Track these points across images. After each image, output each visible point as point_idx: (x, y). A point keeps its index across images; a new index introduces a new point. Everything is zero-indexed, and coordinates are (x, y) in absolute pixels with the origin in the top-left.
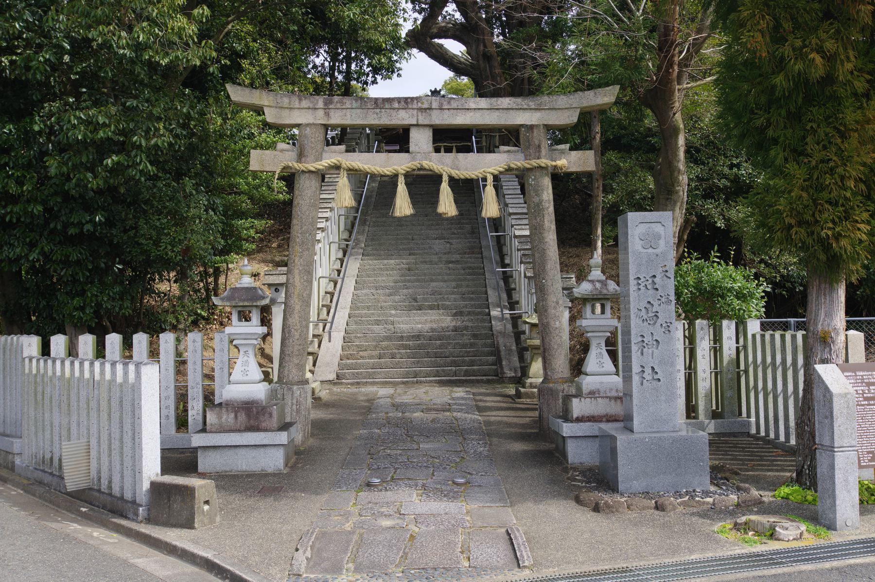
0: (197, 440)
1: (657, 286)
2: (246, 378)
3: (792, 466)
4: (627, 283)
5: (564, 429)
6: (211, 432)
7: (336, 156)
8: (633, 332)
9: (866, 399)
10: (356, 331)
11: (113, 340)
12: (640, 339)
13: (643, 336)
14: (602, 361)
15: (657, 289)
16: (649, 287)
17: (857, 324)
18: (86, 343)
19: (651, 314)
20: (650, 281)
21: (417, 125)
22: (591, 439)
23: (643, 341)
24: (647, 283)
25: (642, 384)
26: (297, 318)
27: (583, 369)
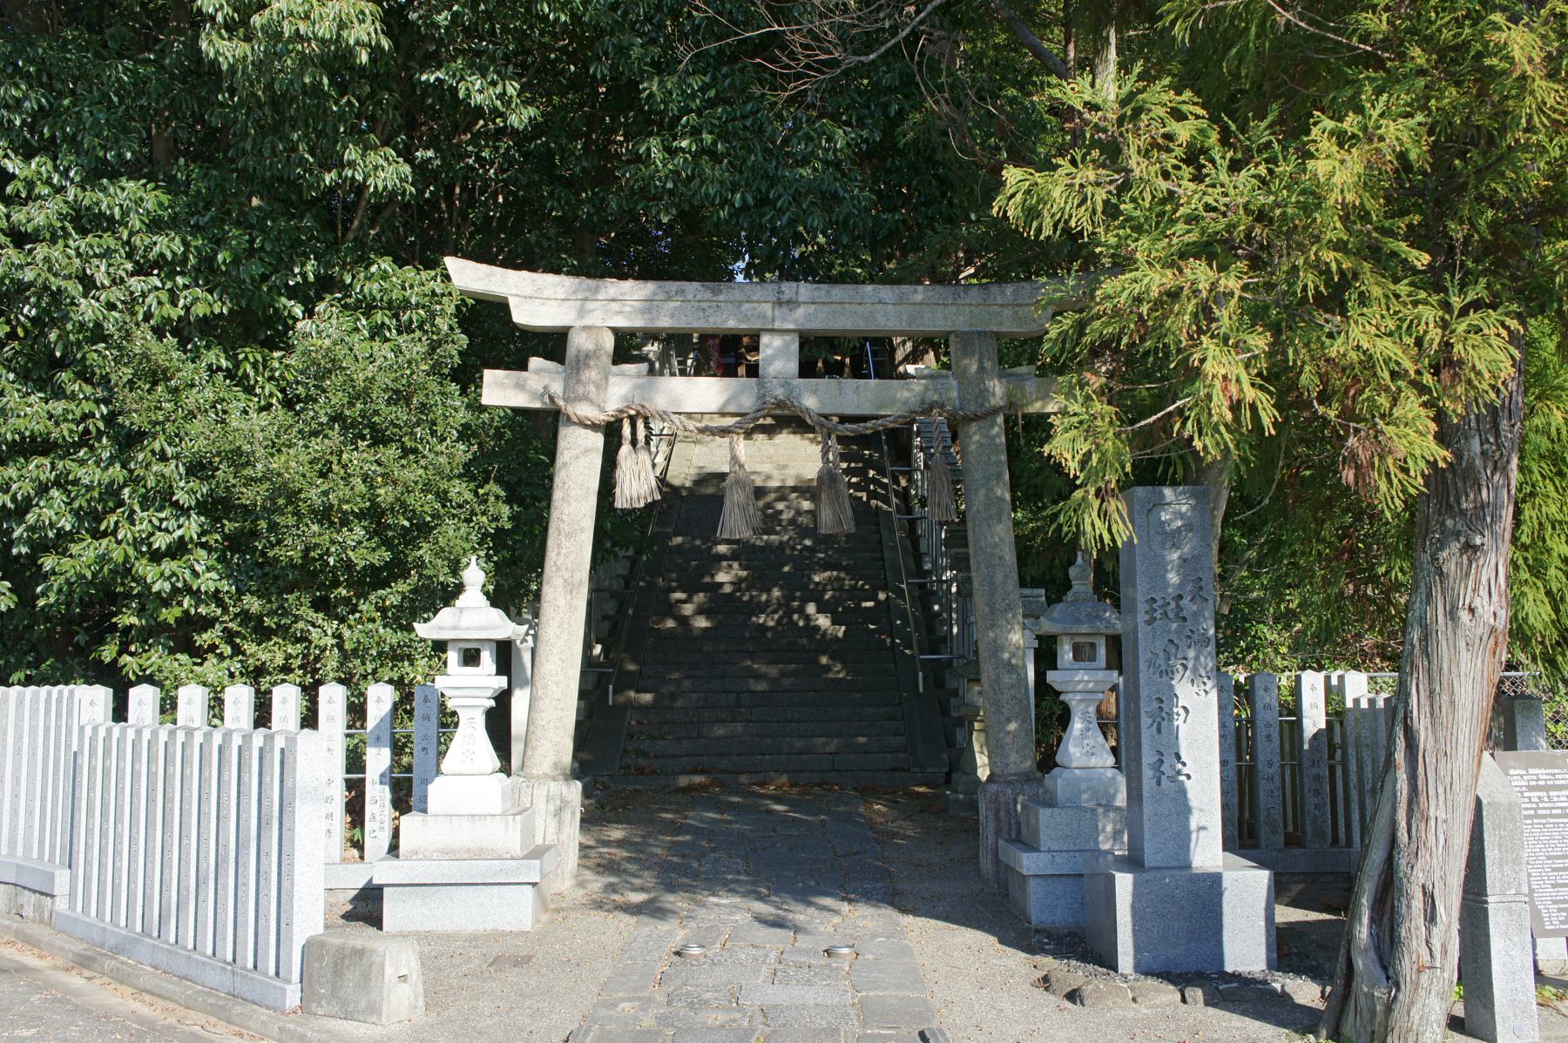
1: (1184, 613)
3: (28, 846)
4: (1133, 611)
5: (1025, 863)
8: (1144, 693)
11: (1364, 705)
15: (1184, 619)
16: (1171, 615)
25: (1159, 784)
27: (1058, 759)
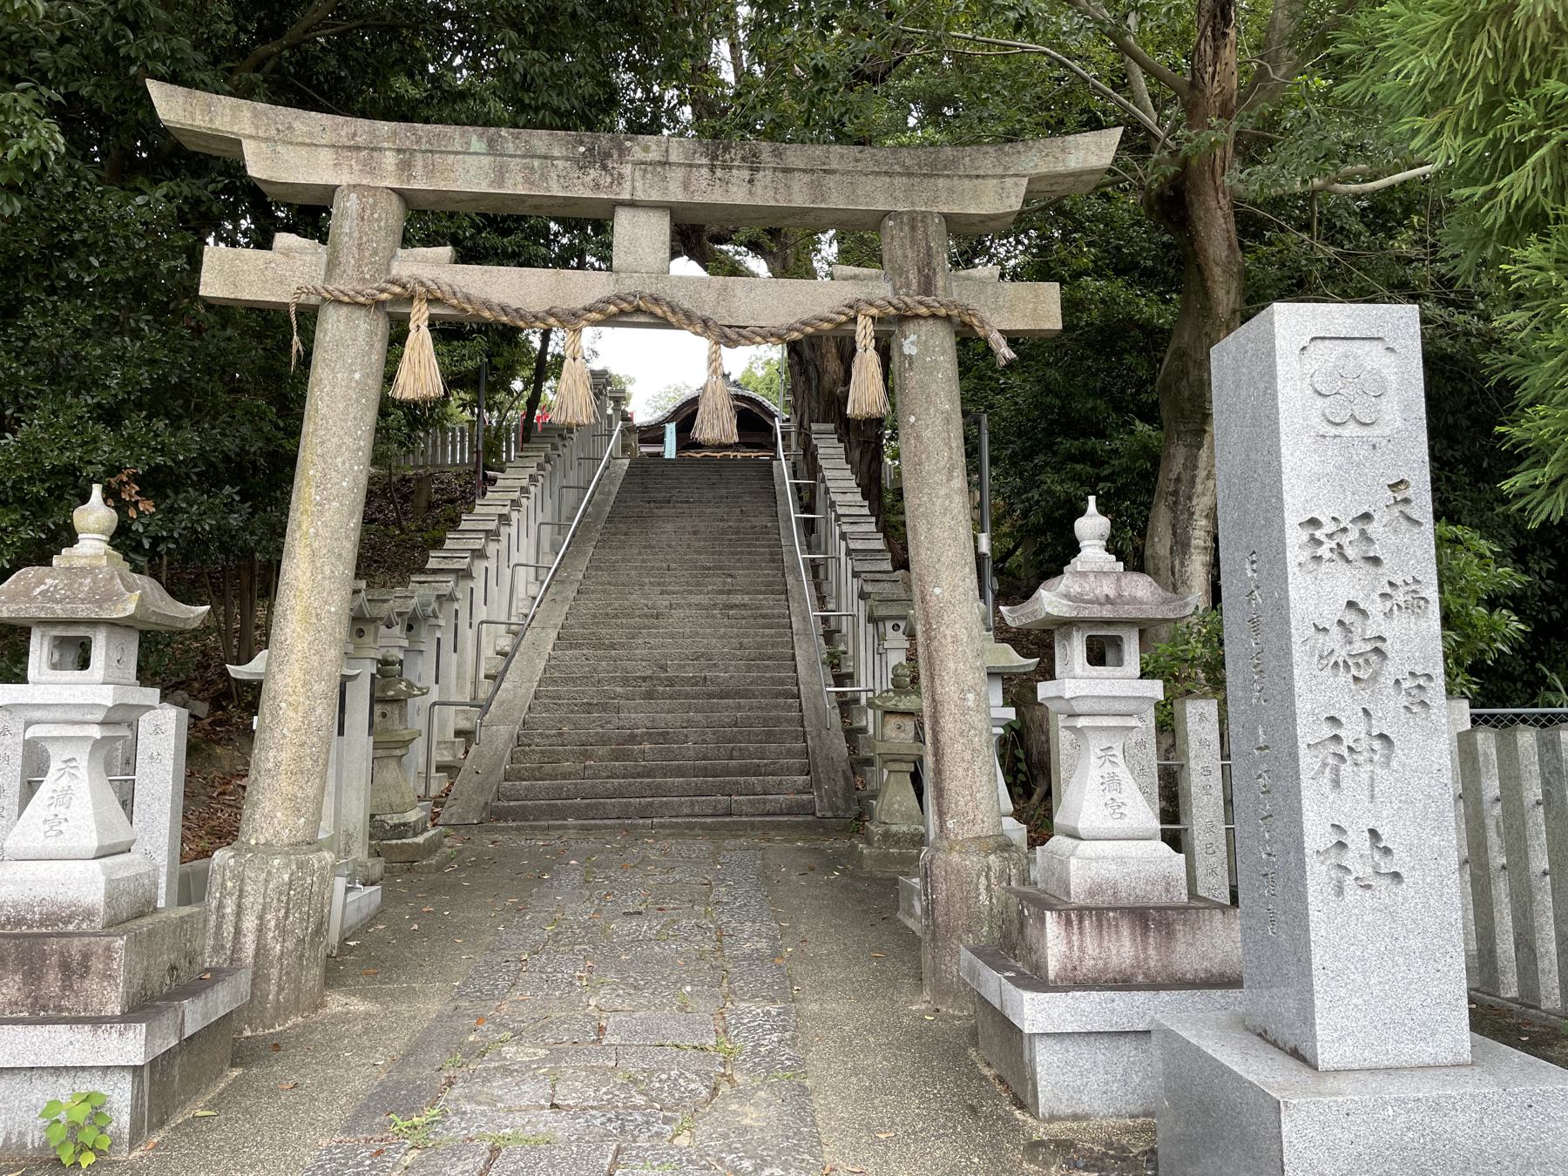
2: (53, 845)
7: (432, 266)
12: (1327, 731)
13: (1333, 720)
14: (1120, 798)
15: (1375, 561)
16: (1350, 552)
17: (1536, 721)
19: (1359, 647)
20: (1354, 534)
21: (632, 204)
22: (1106, 1041)
23: (1336, 738)
24: (1344, 540)
25: (1340, 890)
26: (298, 674)
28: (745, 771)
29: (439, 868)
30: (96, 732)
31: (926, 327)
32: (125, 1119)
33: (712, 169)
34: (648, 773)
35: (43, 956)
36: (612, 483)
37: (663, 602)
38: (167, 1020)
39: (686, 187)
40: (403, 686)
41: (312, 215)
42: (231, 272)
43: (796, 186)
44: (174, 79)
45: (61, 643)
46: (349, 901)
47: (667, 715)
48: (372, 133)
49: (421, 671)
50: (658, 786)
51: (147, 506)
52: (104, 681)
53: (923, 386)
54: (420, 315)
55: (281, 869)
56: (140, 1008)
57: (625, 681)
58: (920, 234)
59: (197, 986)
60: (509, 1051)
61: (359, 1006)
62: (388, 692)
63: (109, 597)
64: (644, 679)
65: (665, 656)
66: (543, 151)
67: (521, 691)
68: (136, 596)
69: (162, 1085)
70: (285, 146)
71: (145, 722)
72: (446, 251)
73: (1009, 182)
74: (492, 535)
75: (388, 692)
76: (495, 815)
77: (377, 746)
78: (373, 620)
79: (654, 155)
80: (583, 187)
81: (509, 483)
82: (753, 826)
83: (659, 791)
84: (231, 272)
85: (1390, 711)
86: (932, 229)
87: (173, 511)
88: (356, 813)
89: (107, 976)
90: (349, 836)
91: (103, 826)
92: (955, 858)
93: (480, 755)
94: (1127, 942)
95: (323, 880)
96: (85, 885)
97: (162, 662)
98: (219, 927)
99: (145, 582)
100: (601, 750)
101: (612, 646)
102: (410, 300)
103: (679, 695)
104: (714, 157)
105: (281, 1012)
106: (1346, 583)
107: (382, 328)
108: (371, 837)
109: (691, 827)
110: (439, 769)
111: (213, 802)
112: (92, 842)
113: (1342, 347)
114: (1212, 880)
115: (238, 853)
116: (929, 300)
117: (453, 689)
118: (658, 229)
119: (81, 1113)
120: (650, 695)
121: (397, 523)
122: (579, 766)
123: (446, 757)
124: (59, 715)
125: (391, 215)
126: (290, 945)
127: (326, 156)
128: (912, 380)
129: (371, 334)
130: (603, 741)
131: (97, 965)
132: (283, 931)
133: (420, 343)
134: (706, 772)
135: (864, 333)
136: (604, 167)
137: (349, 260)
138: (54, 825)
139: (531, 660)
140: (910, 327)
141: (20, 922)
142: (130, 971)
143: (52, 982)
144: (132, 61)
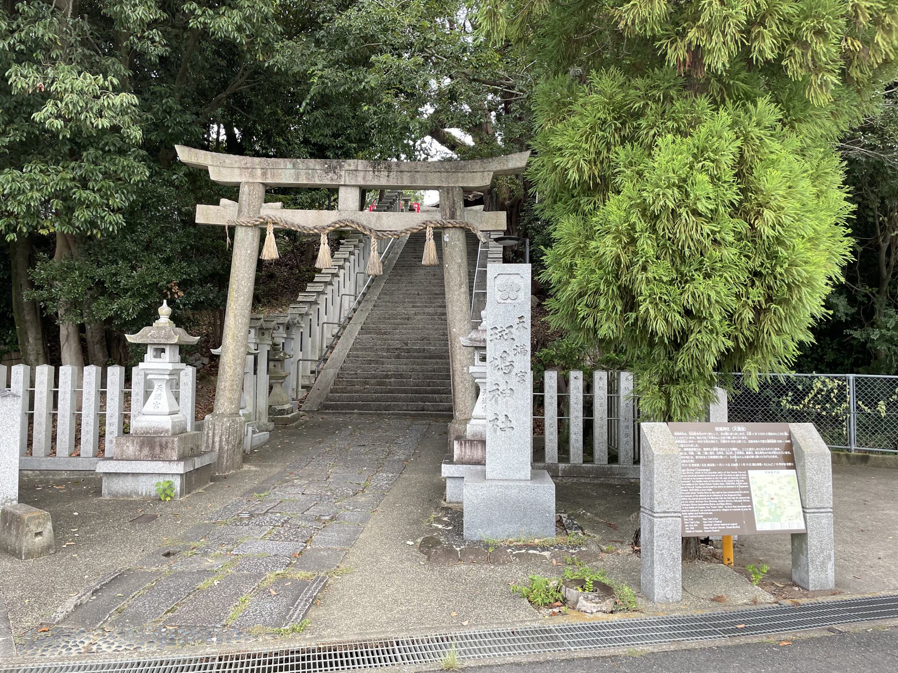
0: (103, 467)
2: (156, 410)
6: (111, 459)
7: (275, 211)
9: (697, 461)
10: (349, 369)
18: (42, 373)
25: (495, 431)
28: (434, 392)
29: (297, 427)
30: (167, 377)
31: (452, 231)
32: (178, 489)
33: (374, 172)
34: (391, 392)
35: (155, 442)
36: (399, 248)
37: (412, 311)
38: (190, 462)
39: (364, 179)
40: (282, 354)
41: (232, 192)
42: (205, 215)
43: (405, 177)
44: (187, 144)
45: (156, 349)
46: (253, 438)
47: (403, 366)
48: (253, 163)
49: (293, 347)
50: (394, 397)
51: (181, 294)
52: (168, 361)
53: (451, 253)
54: (270, 229)
55: (227, 422)
56: (182, 458)
57: (388, 350)
58: (450, 195)
59: (200, 454)
60: (296, 481)
61: (253, 468)
62: (276, 357)
63: (170, 337)
64: (397, 349)
65: (408, 338)
66: (312, 167)
67: (341, 354)
68: (179, 335)
69: (191, 480)
70: (223, 168)
71: (182, 373)
72: (279, 204)
73: (486, 174)
74: (327, 284)
75: (276, 357)
76: (324, 407)
77: (271, 378)
78: (267, 329)
79: (352, 168)
80: (327, 180)
81: (339, 256)
82: (431, 415)
83: (395, 399)
84: (205, 215)
85: (514, 381)
86: (455, 193)
87: (190, 294)
88: (263, 403)
89: (173, 449)
90: (260, 413)
91: (170, 406)
92: (457, 426)
93: (321, 381)
94: (480, 451)
95: (241, 426)
96: (166, 423)
97: (186, 353)
98: (207, 440)
99: (180, 330)
100: (373, 381)
101: (385, 333)
102: (267, 223)
103: (411, 357)
104: (374, 168)
105: (228, 468)
106: (505, 345)
107: (257, 233)
108: (269, 414)
109: (405, 415)
110: (303, 387)
111: (205, 400)
112: (167, 410)
113: (507, 277)
114: (551, 437)
115: (213, 416)
116: (451, 221)
117: (309, 354)
118: (355, 194)
119: (166, 485)
120: (398, 357)
121: (297, 267)
122: (362, 388)
123: (307, 383)
124: (156, 372)
125: (260, 192)
126: (230, 447)
127: (237, 171)
128: (447, 250)
129: (253, 236)
130: (374, 377)
131: (170, 445)
132: (228, 442)
133: (270, 239)
134: (416, 392)
135: (429, 233)
136: (335, 172)
137: (245, 210)
138: (156, 405)
139: (348, 339)
140: (447, 231)
141: (148, 433)
142: (179, 448)
143: (157, 450)
144: (170, 128)
